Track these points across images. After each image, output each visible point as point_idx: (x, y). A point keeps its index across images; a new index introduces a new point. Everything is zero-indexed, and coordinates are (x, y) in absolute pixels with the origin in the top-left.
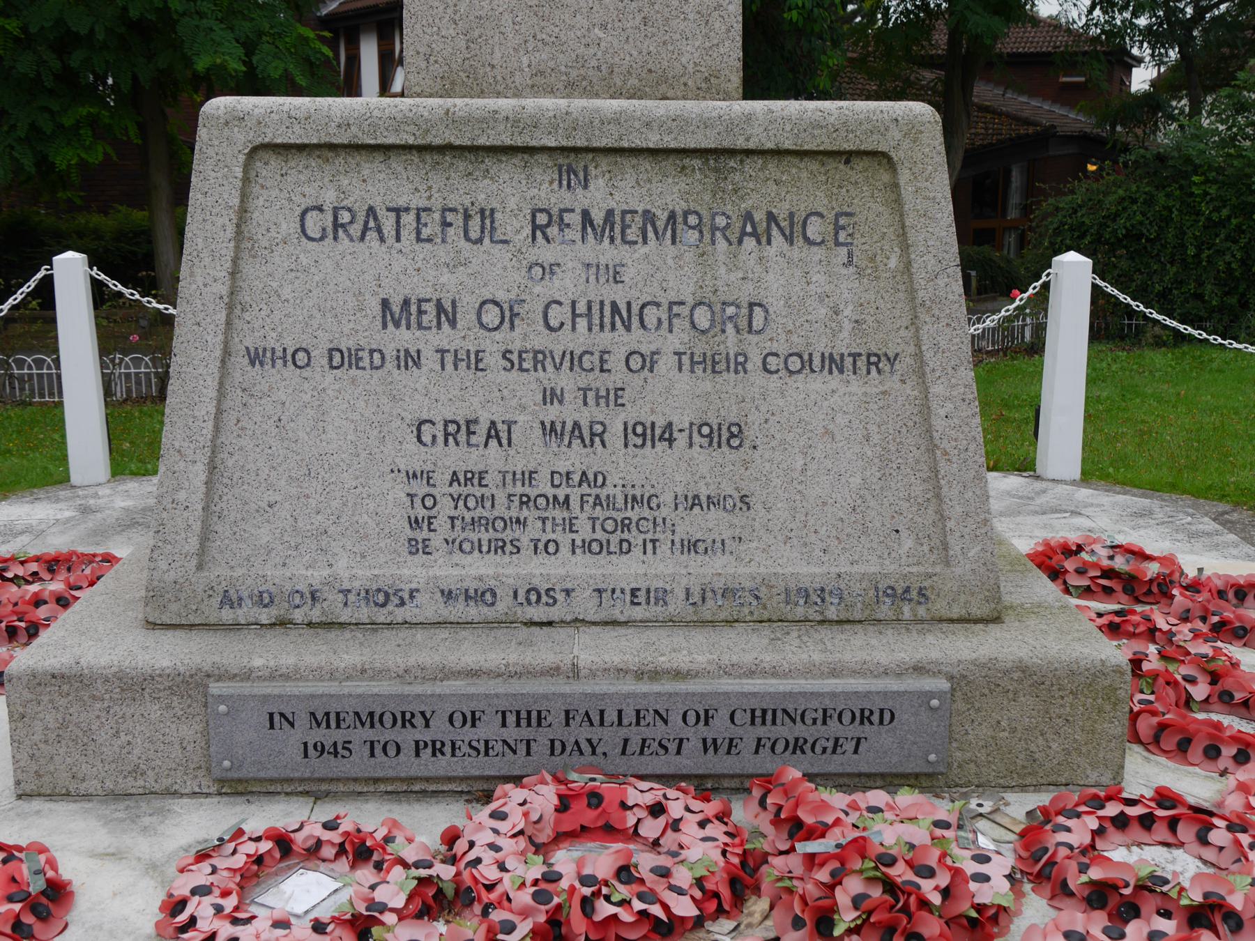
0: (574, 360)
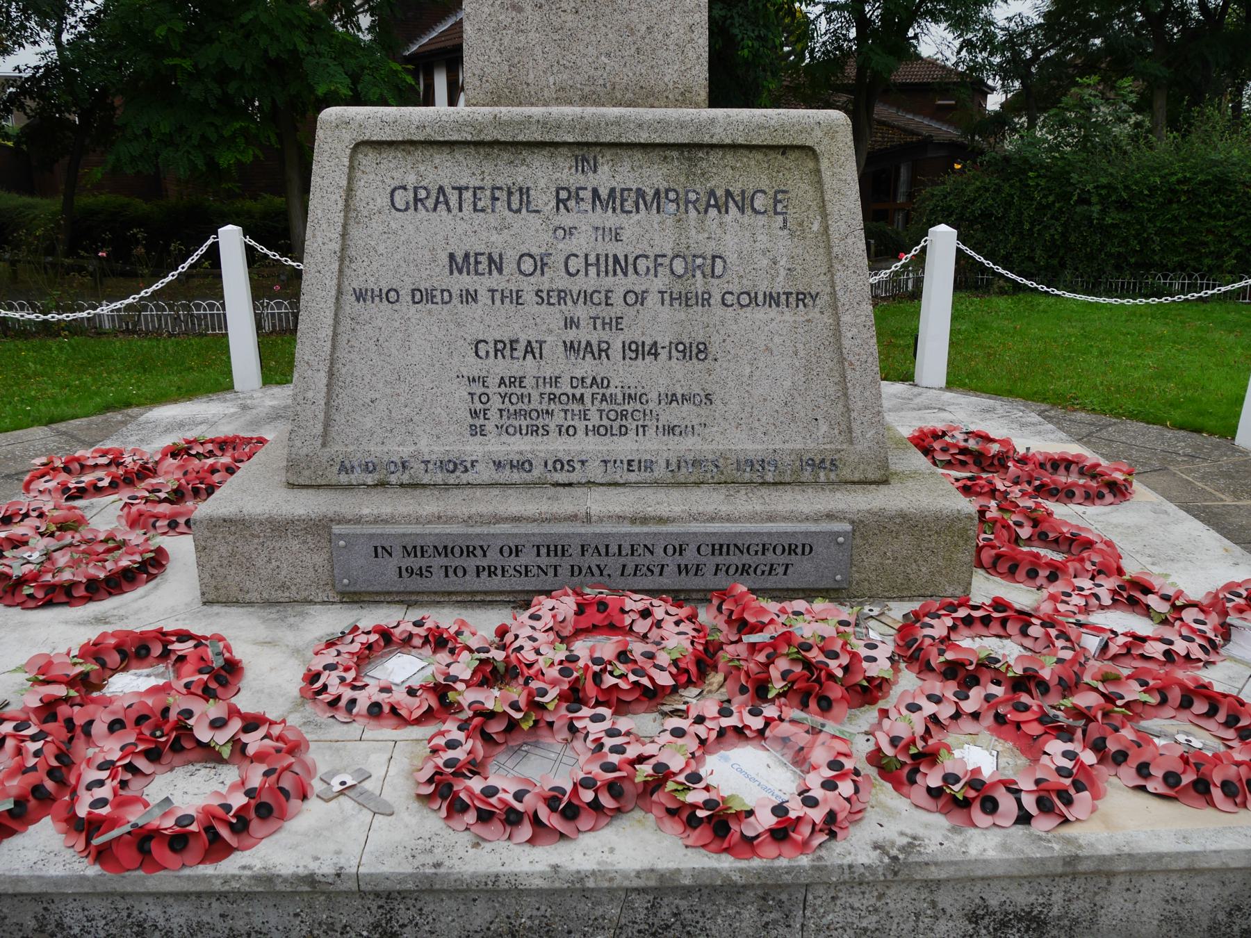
0: (588, 297)
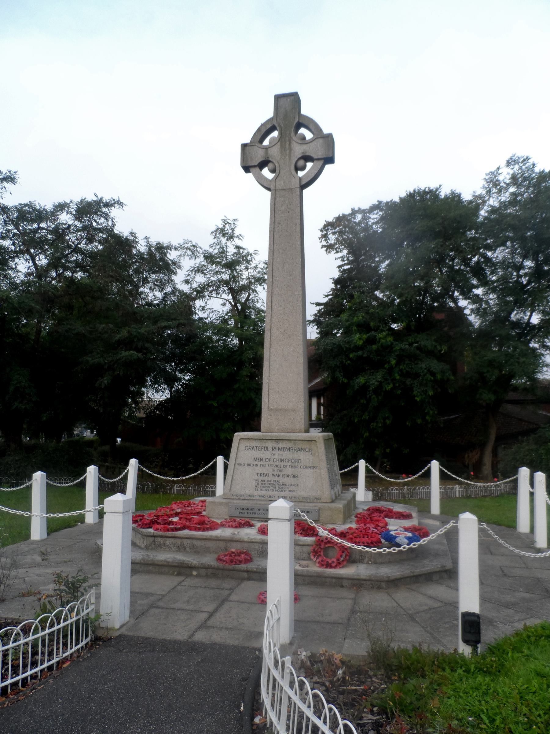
0: (277, 466)
